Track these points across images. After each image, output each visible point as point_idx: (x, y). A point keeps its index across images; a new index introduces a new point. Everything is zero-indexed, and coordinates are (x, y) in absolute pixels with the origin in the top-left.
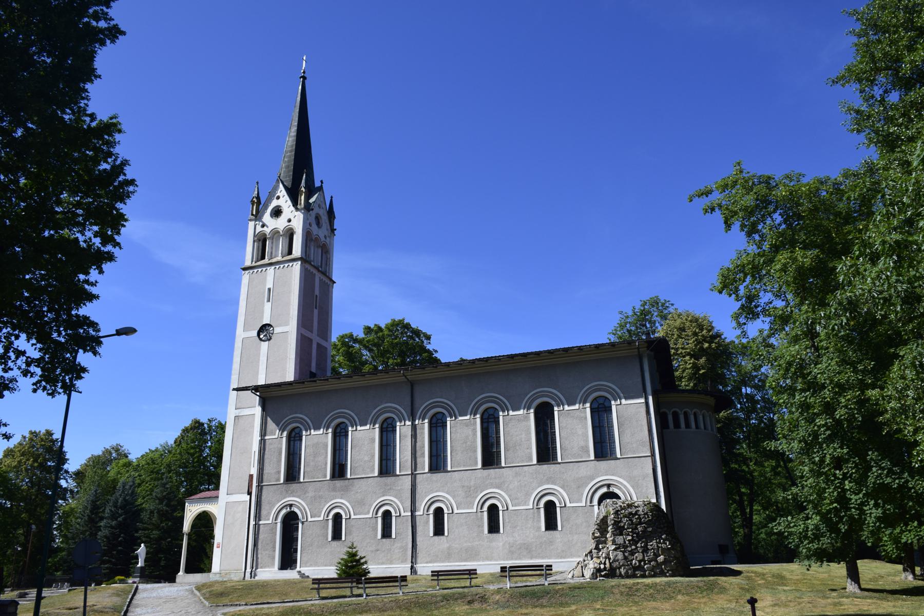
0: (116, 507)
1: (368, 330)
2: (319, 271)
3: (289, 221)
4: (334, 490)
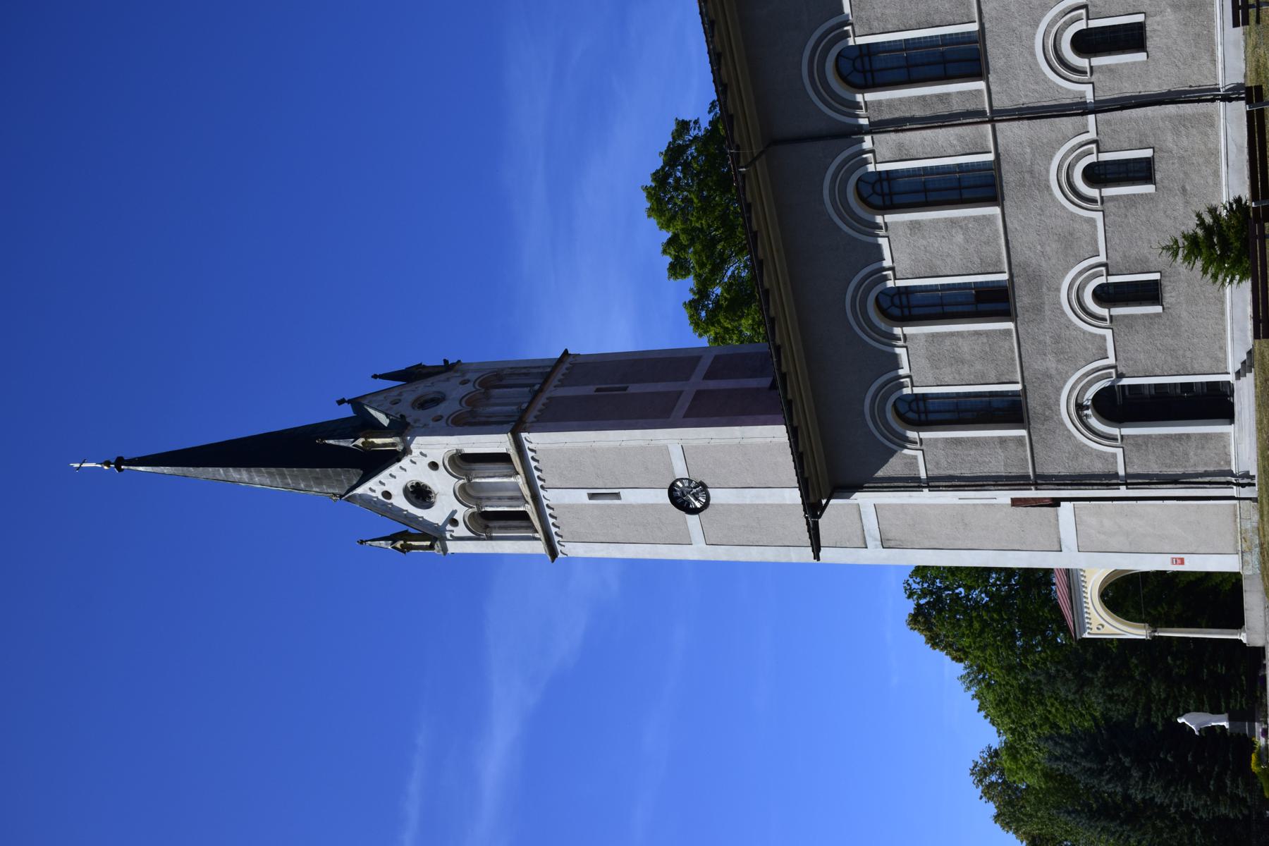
0: (1100, 773)
1: (678, 268)
2: (541, 390)
3: (434, 466)
4: (1038, 309)
